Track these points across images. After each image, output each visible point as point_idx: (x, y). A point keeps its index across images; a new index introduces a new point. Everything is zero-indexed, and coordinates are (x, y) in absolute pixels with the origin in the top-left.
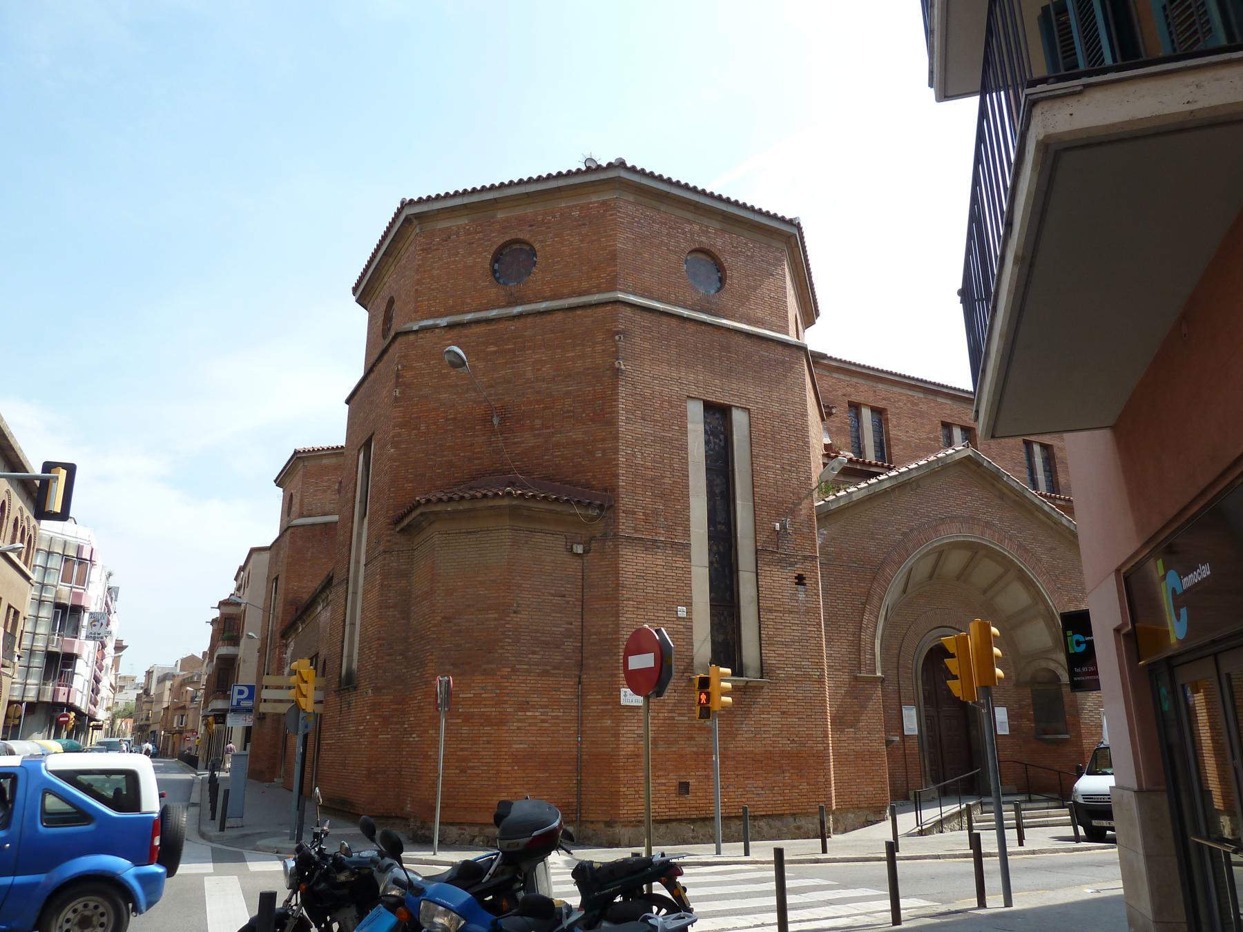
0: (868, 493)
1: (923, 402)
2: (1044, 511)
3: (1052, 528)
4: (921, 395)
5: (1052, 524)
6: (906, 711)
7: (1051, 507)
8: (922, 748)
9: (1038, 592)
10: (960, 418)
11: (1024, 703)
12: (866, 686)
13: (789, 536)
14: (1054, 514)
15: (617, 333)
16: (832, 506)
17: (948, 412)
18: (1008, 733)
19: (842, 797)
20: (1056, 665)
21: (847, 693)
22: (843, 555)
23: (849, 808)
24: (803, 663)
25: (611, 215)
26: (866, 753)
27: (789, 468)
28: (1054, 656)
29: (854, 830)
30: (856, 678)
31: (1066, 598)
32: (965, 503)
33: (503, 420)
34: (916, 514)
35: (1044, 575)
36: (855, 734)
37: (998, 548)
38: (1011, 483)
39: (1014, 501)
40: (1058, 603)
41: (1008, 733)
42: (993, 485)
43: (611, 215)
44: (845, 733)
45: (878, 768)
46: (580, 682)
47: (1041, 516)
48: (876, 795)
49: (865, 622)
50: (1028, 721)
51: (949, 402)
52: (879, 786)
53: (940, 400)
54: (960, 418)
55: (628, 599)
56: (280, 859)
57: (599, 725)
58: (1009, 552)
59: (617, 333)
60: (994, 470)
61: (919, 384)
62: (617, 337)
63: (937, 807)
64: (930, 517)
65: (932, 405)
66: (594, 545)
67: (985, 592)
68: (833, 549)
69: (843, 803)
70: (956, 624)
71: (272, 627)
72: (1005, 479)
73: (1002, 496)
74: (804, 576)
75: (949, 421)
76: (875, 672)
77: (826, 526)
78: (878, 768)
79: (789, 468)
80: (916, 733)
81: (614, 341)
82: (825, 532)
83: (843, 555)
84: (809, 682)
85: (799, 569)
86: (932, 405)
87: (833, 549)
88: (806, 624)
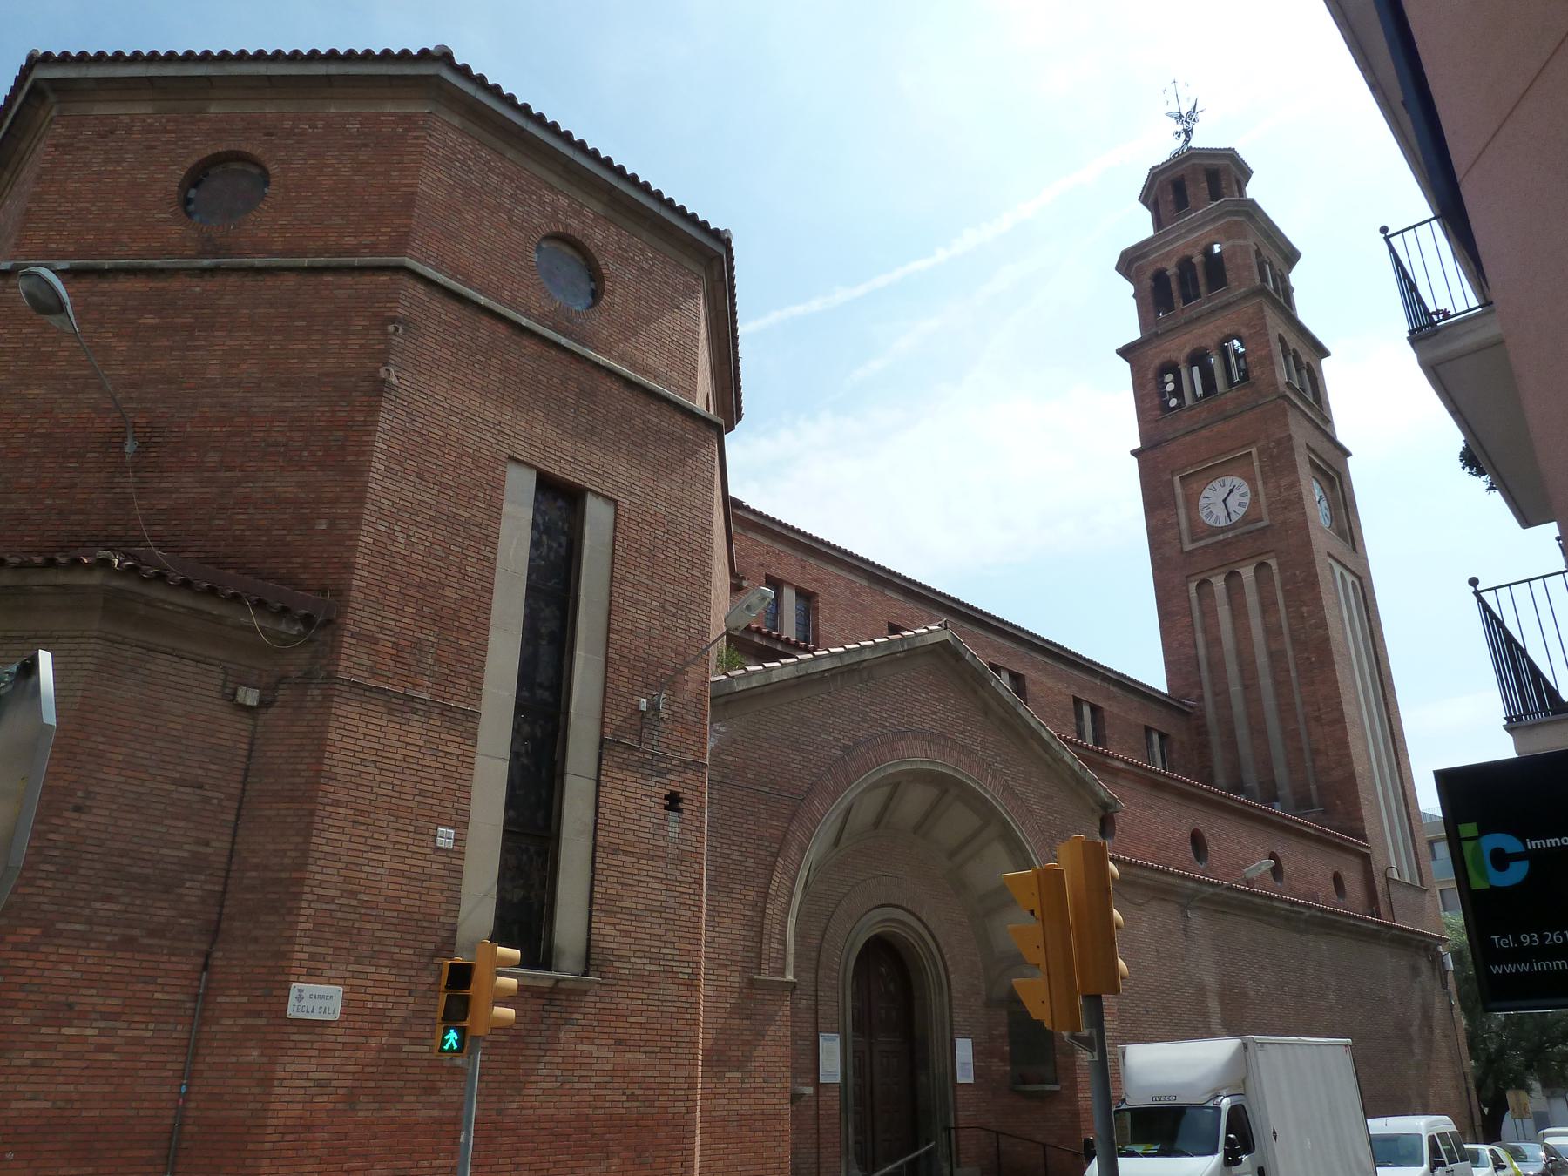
6: (825, 1044)
13: (662, 725)
15: (393, 320)
17: (899, 612)
18: (971, 1080)
25: (416, 138)
27: (674, 610)
30: (752, 983)
33: (145, 446)
41: (971, 1080)
43: (416, 138)
46: (205, 967)
53: (888, 593)
55: (337, 803)
57: (234, 1059)
59: (393, 320)
61: (863, 566)
62: (391, 328)
66: (283, 693)
73: (986, 711)
74: (681, 795)
75: (898, 623)
78: (775, 1144)
79: (674, 610)
81: (386, 333)
82: (722, 729)
85: (673, 782)
87: (733, 759)
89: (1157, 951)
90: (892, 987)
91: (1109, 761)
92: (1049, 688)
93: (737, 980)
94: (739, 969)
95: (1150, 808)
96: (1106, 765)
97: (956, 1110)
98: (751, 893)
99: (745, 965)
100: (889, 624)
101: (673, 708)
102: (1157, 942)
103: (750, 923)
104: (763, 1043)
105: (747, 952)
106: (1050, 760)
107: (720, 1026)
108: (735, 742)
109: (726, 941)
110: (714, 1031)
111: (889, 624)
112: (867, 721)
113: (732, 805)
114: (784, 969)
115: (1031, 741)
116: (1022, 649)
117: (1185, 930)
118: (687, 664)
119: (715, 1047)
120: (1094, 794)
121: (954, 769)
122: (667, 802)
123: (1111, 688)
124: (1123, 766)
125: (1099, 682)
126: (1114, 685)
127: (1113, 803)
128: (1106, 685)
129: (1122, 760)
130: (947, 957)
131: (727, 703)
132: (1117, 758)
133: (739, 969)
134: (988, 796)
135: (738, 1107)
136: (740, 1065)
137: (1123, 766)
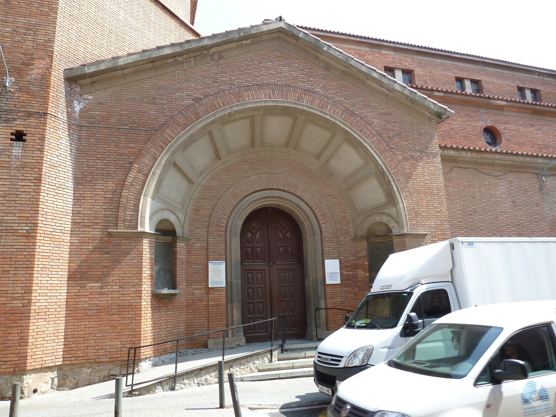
0: (141, 59)
1: (369, 54)
2: (375, 78)
3: (387, 95)
4: (368, 49)
5: (387, 92)
6: (213, 266)
7: (381, 74)
8: (230, 299)
9: (367, 151)
10: (400, 63)
11: (361, 255)
12: (123, 241)
13: (10, 94)
14: (384, 80)
16: (88, 69)
17: (391, 60)
18: (339, 282)
19: (72, 352)
20: (389, 218)
21: (95, 249)
22: (110, 118)
23: (82, 364)
24: (6, 218)
26: (114, 307)
27: (25, 31)
28: (387, 211)
29: (88, 385)
30: (110, 234)
31: (400, 157)
32: (281, 73)
34: (215, 82)
35: (374, 136)
36: (101, 288)
37: (318, 113)
38: (332, 52)
39: (343, 72)
40: (390, 161)
41: (339, 282)
42: (318, 58)
44: (88, 288)
45: (129, 322)
47: (374, 85)
48: (122, 349)
49: (129, 180)
50: (363, 271)
51: (392, 53)
52: (130, 339)
53: (383, 52)
54: (400, 63)
56: (140, 360)
58: (331, 116)
60: (313, 41)
61: (363, 40)
63: (220, 356)
64: (233, 84)
65: (377, 55)
67: (318, 157)
68: (98, 113)
69: (74, 359)
70: (284, 187)
71: (261, 262)
72: (325, 49)
73: (328, 68)
74: (24, 132)
75: (391, 66)
76: (137, 228)
77: (93, 92)
78: (129, 322)
79: (25, 31)
80: (224, 285)
82: (90, 97)
83: (110, 118)
84: (12, 237)
85: (19, 125)
86: (377, 55)
87: (98, 113)
88: (19, 179)
89: (514, 202)
90: (288, 235)
91: (492, 101)
92: (500, 84)
93: (99, 233)
94: (101, 227)
95: (532, 126)
96: (491, 104)
97: (326, 299)
98: (111, 185)
99: (104, 224)
100: (385, 67)
101: (19, 85)
102: (513, 197)
103: (110, 202)
104: (119, 266)
105: (107, 217)
106: (387, 92)
107: (83, 259)
108: (100, 103)
109: (90, 212)
110: (79, 262)
111: (385, 67)
112: (217, 82)
113: (97, 138)
114: (137, 225)
115: (368, 82)
116: (478, 67)
117: (541, 188)
118: (33, 59)
119: (79, 270)
120: (428, 109)
121: (295, 103)
122: (24, 137)
123: (545, 79)
124: (504, 103)
125: (536, 77)
126: (547, 77)
127: (444, 111)
128: (542, 78)
129: (502, 100)
130: (318, 215)
131: (92, 83)
132: (498, 99)
133: (101, 227)
134: (327, 117)
135: (97, 302)
136: (101, 278)
137: (504, 103)
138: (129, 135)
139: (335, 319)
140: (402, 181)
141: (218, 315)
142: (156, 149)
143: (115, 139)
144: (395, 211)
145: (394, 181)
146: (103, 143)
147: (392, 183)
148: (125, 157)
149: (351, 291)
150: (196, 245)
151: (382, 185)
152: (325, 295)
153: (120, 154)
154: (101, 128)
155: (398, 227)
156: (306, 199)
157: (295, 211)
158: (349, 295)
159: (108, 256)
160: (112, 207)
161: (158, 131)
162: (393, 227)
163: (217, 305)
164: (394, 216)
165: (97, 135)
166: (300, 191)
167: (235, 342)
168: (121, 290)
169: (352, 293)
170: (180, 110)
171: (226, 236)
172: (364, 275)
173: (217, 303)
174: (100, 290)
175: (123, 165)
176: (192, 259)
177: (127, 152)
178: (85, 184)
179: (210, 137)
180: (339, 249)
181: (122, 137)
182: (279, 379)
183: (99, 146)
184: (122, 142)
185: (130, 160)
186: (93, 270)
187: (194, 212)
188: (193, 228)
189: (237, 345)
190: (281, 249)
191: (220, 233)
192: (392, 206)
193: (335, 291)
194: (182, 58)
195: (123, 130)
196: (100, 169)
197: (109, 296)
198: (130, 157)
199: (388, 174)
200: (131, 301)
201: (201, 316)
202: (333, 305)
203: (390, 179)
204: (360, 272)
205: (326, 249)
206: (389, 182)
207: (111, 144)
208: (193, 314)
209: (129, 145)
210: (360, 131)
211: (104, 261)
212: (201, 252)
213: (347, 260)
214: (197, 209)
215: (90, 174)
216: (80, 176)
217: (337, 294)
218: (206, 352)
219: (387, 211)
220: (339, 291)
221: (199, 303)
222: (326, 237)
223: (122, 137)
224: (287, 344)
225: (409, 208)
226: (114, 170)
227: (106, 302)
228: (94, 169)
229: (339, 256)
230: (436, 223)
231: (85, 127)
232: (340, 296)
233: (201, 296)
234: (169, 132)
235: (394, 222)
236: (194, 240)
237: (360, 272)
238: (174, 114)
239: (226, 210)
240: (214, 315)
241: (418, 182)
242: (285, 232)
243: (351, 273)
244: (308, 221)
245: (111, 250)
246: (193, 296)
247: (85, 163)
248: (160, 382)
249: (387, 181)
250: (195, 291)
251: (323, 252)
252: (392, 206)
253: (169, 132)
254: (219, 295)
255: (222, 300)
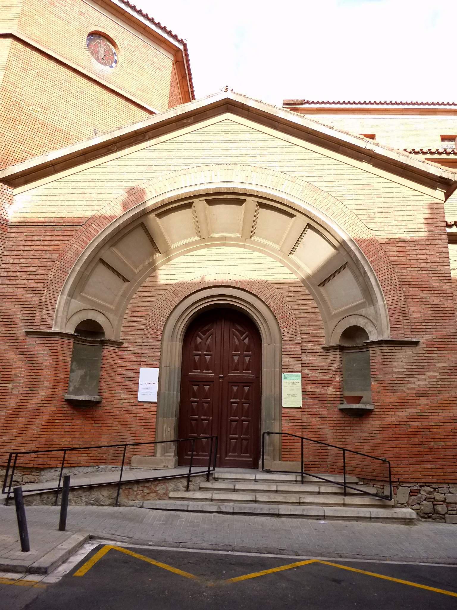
20: (366, 320)
28: (363, 311)
97: (281, 420)
138: (55, 232)
139: (291, 447)
140: (383, 272)
141: (146, 430)
142: (79, 245)
143: (41, 237)
144: (373, 311)
145: (371, 271)
146: (29, 242)
147: (369, 274)
148: (48, 255)
149: (317, 413)
150: (129, 349)
151: (356, 278)
152: (280, 416)
153: (44, 252)
154: (29, 227)
155: (376, 331)
156: (264, 297)
157: (250, 312)
158: (314, 419)
159: (22, 356)
160: (30, 306)
161: (83, 226)
162: (370, 332)
163: (146, 419)
164: (371, 318)
165: (25, 234)
166: (256, 288)
167: (163, 462)
168: (30, 392)
169: (319, 416)
170: (108, 202)
171: (162, 340)
172: (334, 393)
173: (146, 416)
174: (10, 391)
175: (46, 263)
176: (124, 365)
177: (51, 249)
178: (9, 283)
179: (145, 232)
180: (304, 359)
181: (48, 234)
182: (188, 511)
183: (25, 244)
184: (47, 239)
185: (53, 258)
186: (6, 370)
187: (130, 312)
188: (128, 330)
189: (164, 466)
190: (236, 358)
191: (156, 336)
192: (369, 304)
193: (294, 413)
194: (116, 147)
195: (50, 227)
196: (23, 268)
197: (19, 398)
198: (54, 255)
199: (363, 262)
200: (39, 405)
201: (128, 429)
202: (291, 430)
203: (366, 268)
204: (331, 390)
205: (285, 359)
206: (365, 273)
207: (37, 242)
208: (119, 426)
209: (53, 242)
210: (327, 210)
211: (17, 362)
212: (134, 357)
213: (314, 374)
214: (133, 310)
215: (15, 272)
216: (5, 275)
217: (297, 415)
218: (127, 471)
219: (364, 312)
220: (299, 413)
221: (127, 415)
222: (286, 344)
223: (48, 234)
224: (218, 473)
225: (392, 307)
226: (37, 268)
227: (14, 404)
228: (18, 268)
229: (303, 368)
230: (435, 327)
231: (15, 227)
232: (300, 418)
233: (130, 407)
234: (95, 226)
235: (372, 325)
236: (127, 344)
237: (331, 390)
238: (102, 207)
239: (164, 311)
240: (142, 430)
241: (409, 272)
242: (242, 338)
243: (319, 391)
244: (264, 325)
245: (25, 350)
246: (121, 406)
247: (11, 262)
248: (40, 494)
249: (362, 271)
250: (124, 401)
251: (281, 363)
252: (369, 304)
253: (95, 226)
254: (149, 407)
255: (151, 413)
